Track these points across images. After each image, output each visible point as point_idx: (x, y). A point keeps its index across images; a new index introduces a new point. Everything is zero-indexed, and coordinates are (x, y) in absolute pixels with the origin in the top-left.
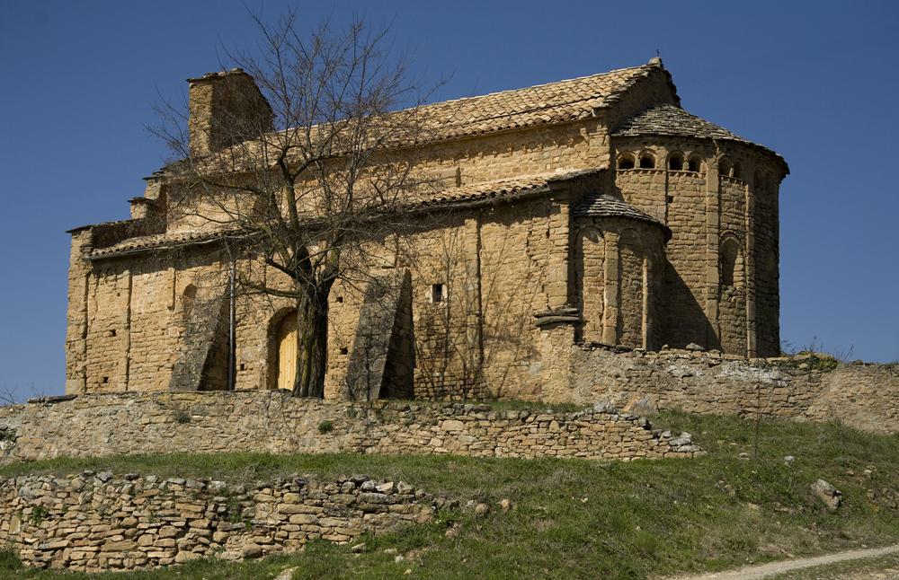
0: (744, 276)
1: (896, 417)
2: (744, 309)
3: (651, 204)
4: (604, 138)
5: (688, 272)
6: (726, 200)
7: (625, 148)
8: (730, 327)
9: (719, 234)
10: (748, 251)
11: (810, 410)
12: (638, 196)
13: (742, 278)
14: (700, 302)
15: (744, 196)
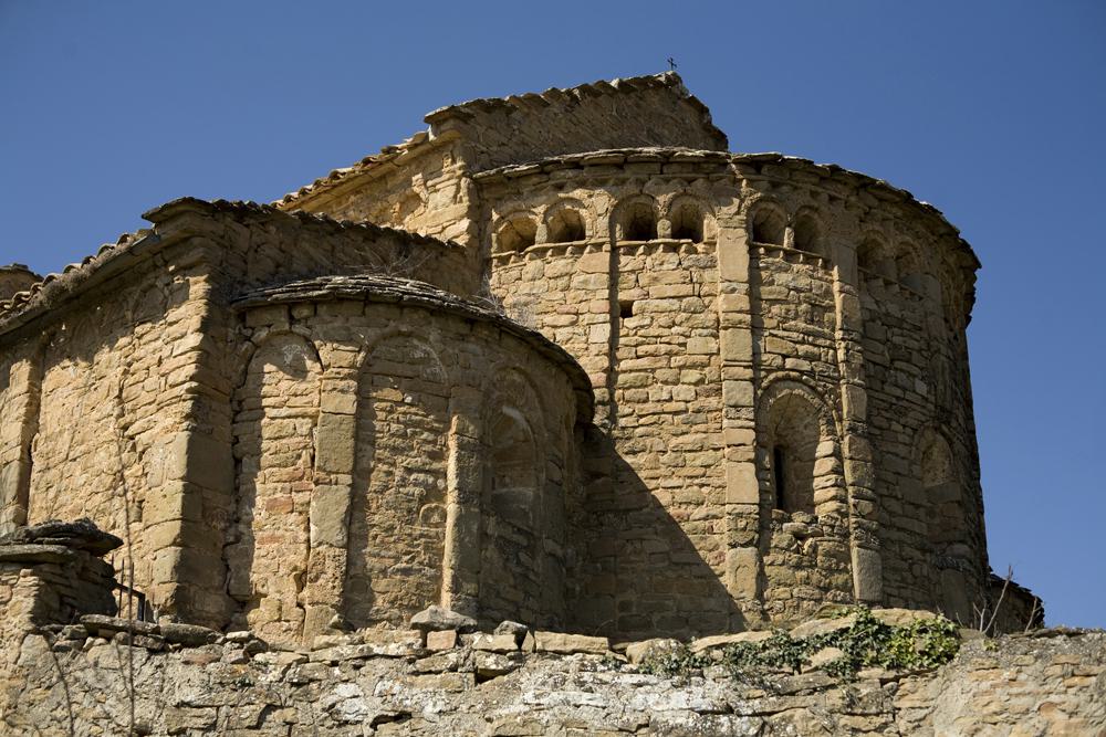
0: (840, 485)
2: (846, 570)
3: (573, 324)
7: (510, 205)
9: (753, 380)
10: (846, 423)
12: (540, 308)
13: (833, 492)
14: (709, 558)
15: (828, 294)
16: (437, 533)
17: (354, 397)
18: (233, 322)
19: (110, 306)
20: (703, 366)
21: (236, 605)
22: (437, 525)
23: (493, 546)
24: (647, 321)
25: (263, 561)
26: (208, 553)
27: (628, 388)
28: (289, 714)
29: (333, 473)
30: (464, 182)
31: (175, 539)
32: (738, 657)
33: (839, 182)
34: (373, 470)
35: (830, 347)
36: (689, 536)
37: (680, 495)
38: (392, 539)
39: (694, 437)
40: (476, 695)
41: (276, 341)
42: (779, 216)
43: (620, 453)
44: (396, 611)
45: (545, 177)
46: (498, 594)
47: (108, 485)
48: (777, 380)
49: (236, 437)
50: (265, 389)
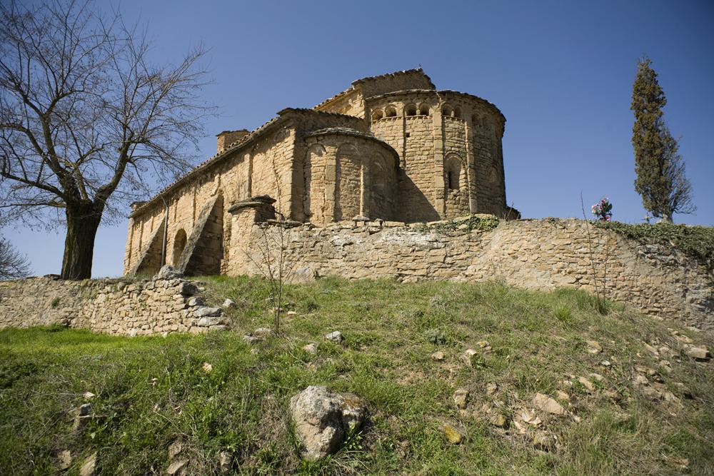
1: (563, 272)
7: (376, 107)
11: (469, 271)
13: (464, 184)
14: (431, 202)
15: (464, 129)
20: (429, 150)
28: (321, 244)
30: (363, 101)
32: (439, 227)
40: (370, 238)
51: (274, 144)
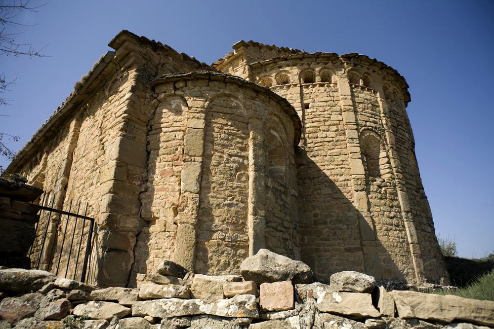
0: (390, 168)
2: (397, 200)
4: (245, 68)
5: (331, 167)
6: (360, 103)
7: (263, 74)
8: (385, 219)
10: (390, 146)
13: (388, 170)
14: (347, 196)
15: (377, 101)
16: (245, 186)
17: (203, 121)
18: (149, 91)
19: (102, 92)
20: (337, 125)
21: (145, 223)
22: (244, 182)
23: (271, 192)
24: (315, 110)
25: (158, 201)
26: (130, 197)
27: (310, 133)
29: (193, 156)
30: (247, 67)
31: (110, 190)
33: (376, 65)
34: (212, 155)
35: (380, 119)
36: (339, 187)
37: (334, 172)
38: (223, 189)
39: (337, 150)
41: (168, 99)
42: (357, 76)
43: (309, 157)
44: (225, 226)
45: (275, 64)
46: (274, 215)
47: (92, 166)
48: (365, 130)
49: (149, 142)
50: (162, 120)
51: (106, 99)
